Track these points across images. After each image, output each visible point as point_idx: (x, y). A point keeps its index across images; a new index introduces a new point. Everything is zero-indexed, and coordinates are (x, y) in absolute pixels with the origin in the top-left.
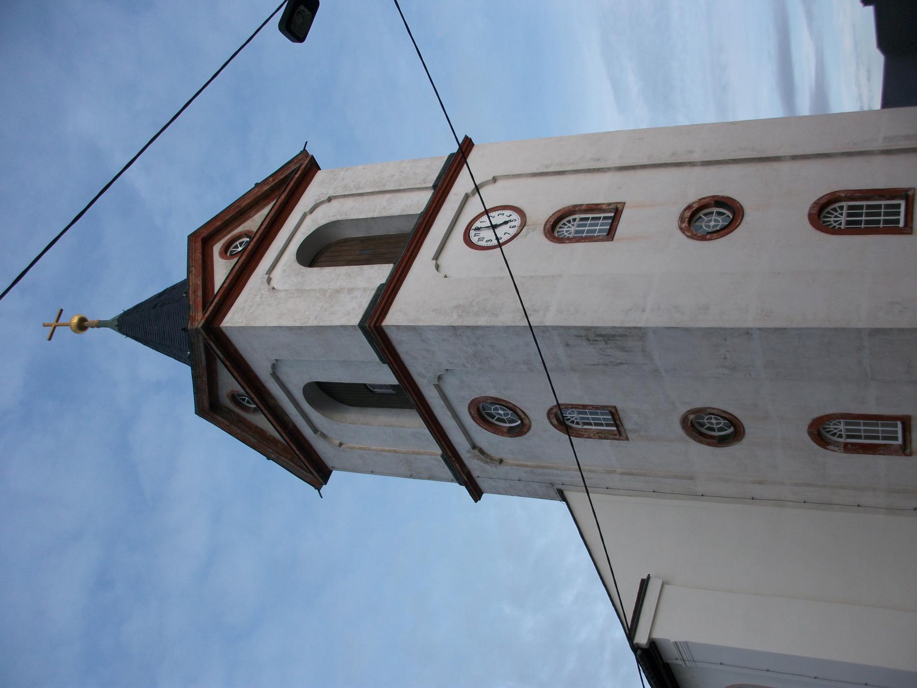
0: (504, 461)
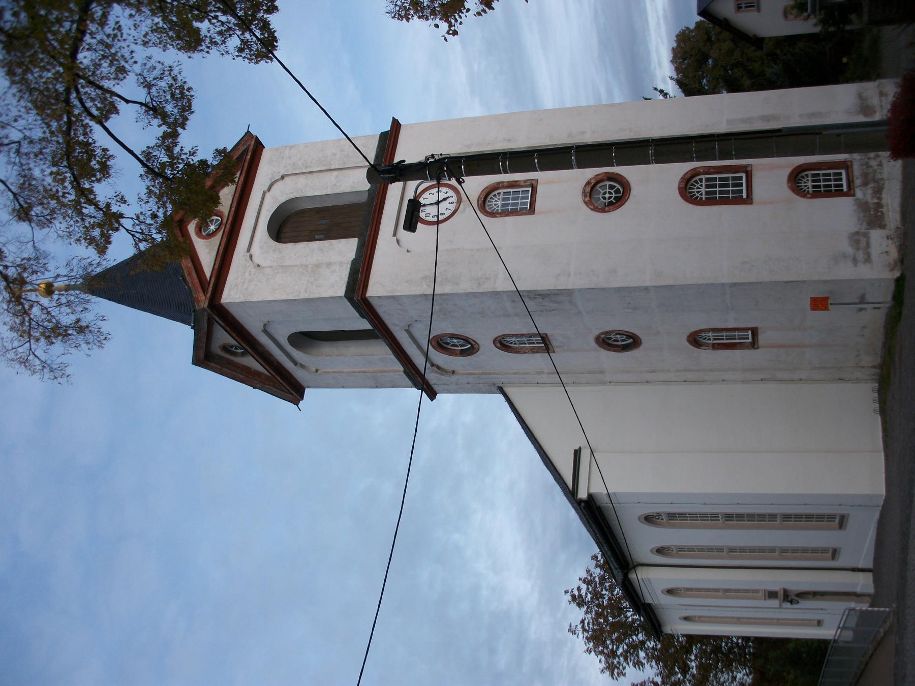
0: (456, 372)
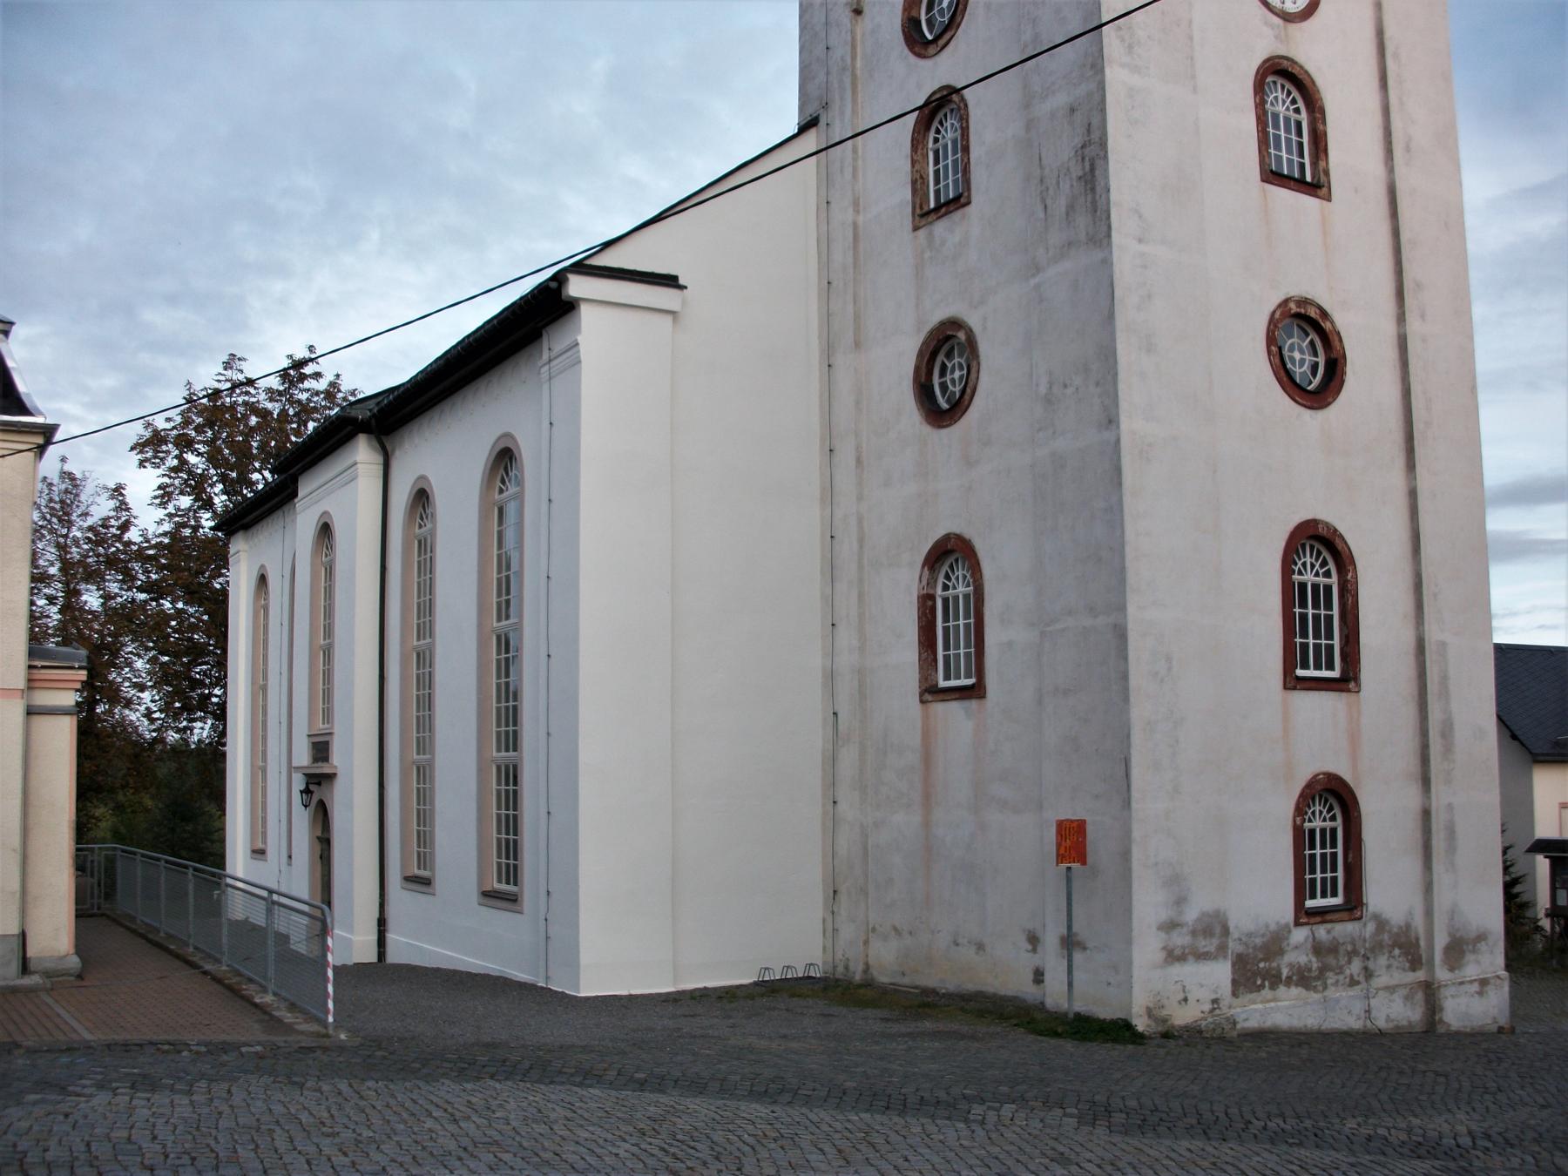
0: (859, 18)
